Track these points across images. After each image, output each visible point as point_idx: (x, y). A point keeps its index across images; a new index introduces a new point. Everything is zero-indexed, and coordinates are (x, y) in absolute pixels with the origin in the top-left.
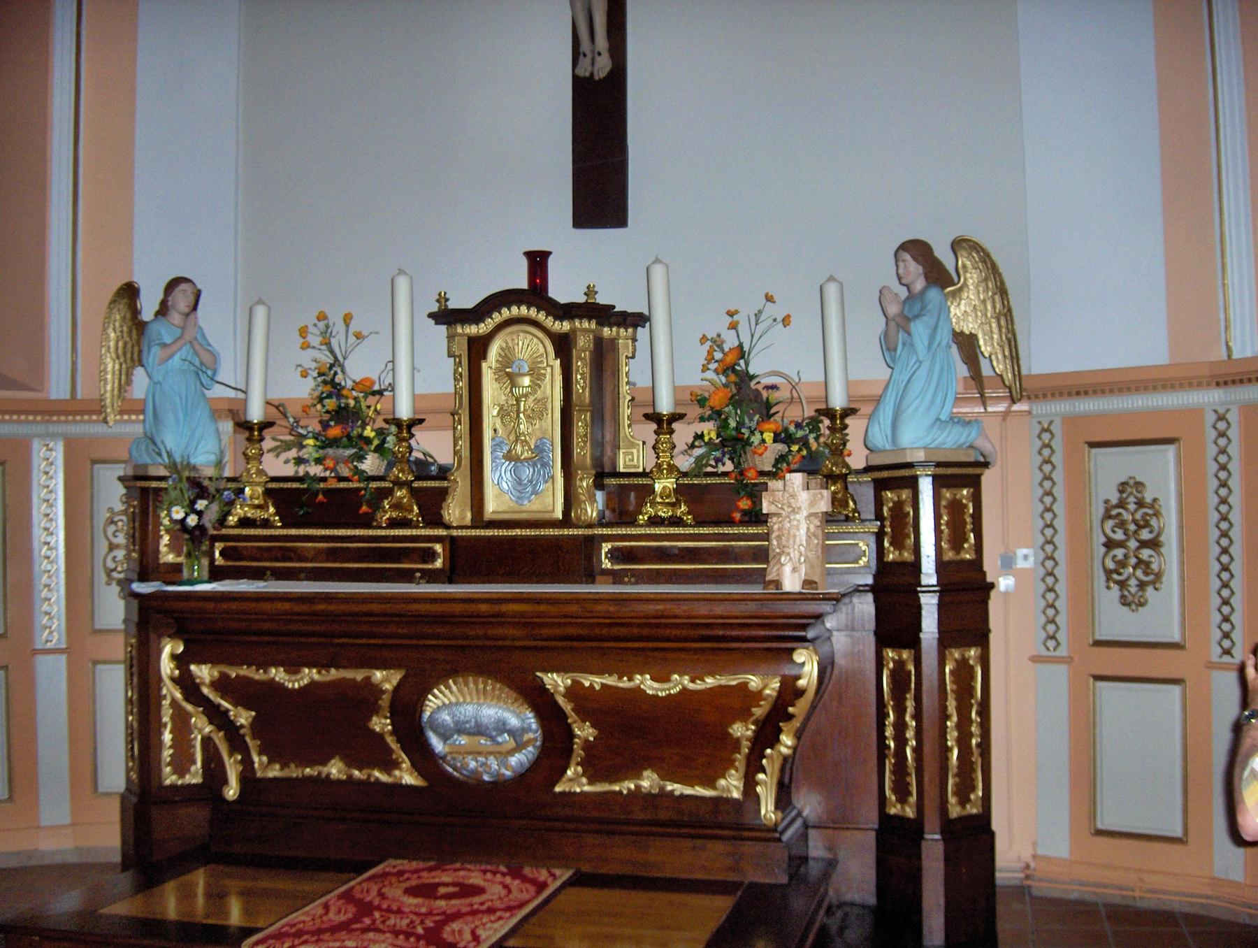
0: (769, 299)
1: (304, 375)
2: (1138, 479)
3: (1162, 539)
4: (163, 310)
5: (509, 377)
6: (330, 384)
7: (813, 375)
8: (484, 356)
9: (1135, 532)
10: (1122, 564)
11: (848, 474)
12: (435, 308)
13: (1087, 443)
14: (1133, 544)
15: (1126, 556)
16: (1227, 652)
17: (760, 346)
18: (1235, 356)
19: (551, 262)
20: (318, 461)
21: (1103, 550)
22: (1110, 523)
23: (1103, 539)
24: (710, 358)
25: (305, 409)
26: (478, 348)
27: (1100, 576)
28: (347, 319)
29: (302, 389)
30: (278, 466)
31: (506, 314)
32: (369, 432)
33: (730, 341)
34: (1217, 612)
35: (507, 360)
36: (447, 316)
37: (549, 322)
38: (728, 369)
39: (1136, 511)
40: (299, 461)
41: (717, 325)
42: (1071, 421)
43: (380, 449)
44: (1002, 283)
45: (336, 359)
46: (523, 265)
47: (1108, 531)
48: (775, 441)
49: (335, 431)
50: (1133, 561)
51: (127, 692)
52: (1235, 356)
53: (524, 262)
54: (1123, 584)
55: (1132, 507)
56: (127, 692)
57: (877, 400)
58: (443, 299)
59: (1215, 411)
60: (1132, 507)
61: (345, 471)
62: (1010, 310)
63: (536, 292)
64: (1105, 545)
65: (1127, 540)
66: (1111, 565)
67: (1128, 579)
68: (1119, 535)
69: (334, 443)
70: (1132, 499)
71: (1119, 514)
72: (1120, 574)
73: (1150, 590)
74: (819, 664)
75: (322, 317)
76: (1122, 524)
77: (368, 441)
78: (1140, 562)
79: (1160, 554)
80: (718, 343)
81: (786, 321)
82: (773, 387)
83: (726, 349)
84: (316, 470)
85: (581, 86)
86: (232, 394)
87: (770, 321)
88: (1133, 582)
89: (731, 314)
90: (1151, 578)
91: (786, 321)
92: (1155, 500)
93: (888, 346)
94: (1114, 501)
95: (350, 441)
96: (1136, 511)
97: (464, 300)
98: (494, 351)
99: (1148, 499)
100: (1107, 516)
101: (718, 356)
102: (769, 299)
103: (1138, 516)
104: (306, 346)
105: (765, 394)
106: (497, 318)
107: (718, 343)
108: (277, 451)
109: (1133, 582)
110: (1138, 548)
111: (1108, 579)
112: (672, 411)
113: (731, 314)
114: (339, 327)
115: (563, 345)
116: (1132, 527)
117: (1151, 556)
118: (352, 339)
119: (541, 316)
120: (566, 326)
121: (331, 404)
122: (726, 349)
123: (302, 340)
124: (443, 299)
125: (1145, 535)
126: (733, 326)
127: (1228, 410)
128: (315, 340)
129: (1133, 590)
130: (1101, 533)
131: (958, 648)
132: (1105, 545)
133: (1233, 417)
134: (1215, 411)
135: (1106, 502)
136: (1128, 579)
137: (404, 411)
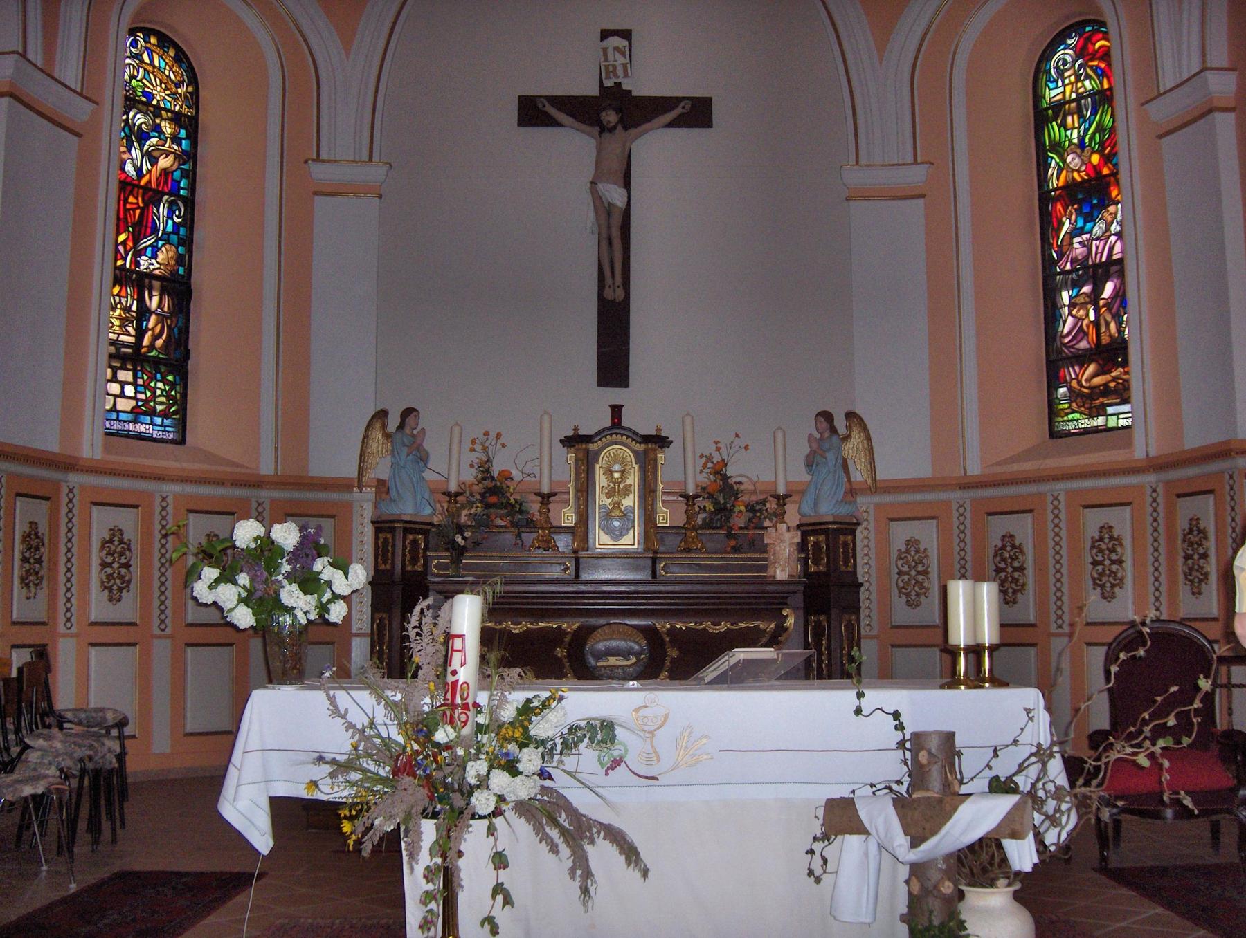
0: (737, 436)
2: (1110, 524)
3: (1208, 553)
4: (401, 427)
7: (767, 477)
9: (1108, 555)
10: (908, 583)
13: (987, 513)
14: (1107, 562)
15: (1104, 570)
16: (1060, 627)
17: (732, 460)
18: (969, 473)
19: (623, 409)
21: (897, 576)
22: (1095, 551)
23: (897, 570)
24: (705, 466)
27: (895, 591)
28: (499, 436)
29: (469, 475)
33: (717, 459)
38: (716, 472)
39: (915, 555)
41: (710, 449)
42: (1069, 493)
44: (869, 434)
45: (489, 457)
47: (900, 566)
48: (747, 511)
50: (914, 582)
52: (969, 473)
53: (609, 410)
54: (907, 595)
55: (1106, 540)
57: (802, 493)
59: (958, 502)
60: (1106, 540)
62: (872, 448)
64: (898, 574)
65: (910, 571)
66: (901, 584)
67: (910, 592)
68: (906, 568)
70: (913, 549)
71: (905, 557)
72: (906, 589)
73: (1019, 595)
76: (1004, 560)
78: (1111, 572)
79: (1024, 574)
80: (709, 458)
81: (746, 448)
82: (740, 483)
83: (715, 462)
86: (439, 478)
87: (737, 447)
88: (913, 593)
89: (717, 443)
90: (1117, 581)
91: (746, 448)
92: (925, 549)
93: (810, 463)
94: (903, 550)
96: (915, 555)
99: (1017, 544)
100: (1093, 547)
101: (710, 465)
102: (737, 436)
103: (1110, 546)
104: (473, 450)
105: (735, 487)
107: (709, 458)
109: (913, 593)
110: (1013, 572)
111: (1095, 584)
112: (694, 493)
113: (717, 443)
116: (913, 564)
117: (1117, 569)
118: (499, 446)
122: (715, 462)
123: (471, 446)
125: (920, 568)
126: (718, 449)
127: (965, 502)
129: (1108, 589)
130: (1089, 556)
132: (898, 574)
133: (968, 506)
134: (958, 502)
135: (1093, 538)
136: (910, 592)
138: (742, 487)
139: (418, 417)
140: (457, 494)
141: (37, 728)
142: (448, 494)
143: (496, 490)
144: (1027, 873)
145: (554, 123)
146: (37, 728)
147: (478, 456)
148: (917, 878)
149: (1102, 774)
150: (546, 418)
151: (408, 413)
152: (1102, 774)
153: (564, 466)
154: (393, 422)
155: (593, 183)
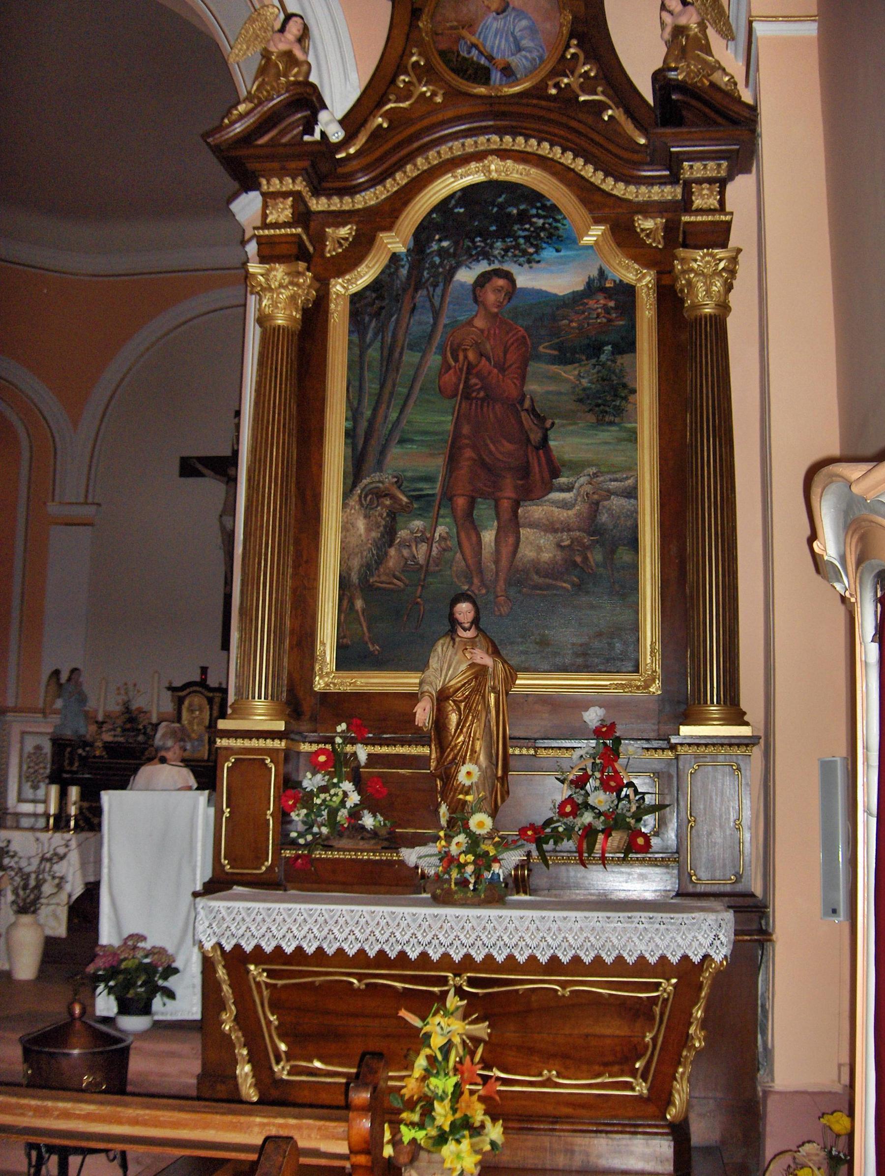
1: (118, 704)
4: (69, 680)
5: (191, 711)
6: (127, 709)
8: (183, 703)
11: (618, 795)
12: (167, 685)
19: (209, 671)
20: (122, 736)
25: (117, 717)
26: (180, 702)
28: (135, 685)
30: (108, 737)
31: (191, 689)
32: (141, 727)
34: (836, 1068)
35: (190, 705)
36: (171, 688)
37: (206, 693)
40: (115, 736)
43: (145, 734)
46: (199, 671)
49: (128, 726)
51: (876, 592)
56: (876, 592)
58: (170, 683)
61: (131, 740)
63: (203, 683)
69: (128, 730)
74: (553, 364)
75: (126, 684)
77: (140, 730)
84: (121, 739)
85: (225, 594)
95: (133, 730)
97: (178, 683)
98: (186, 703)
104: (119, 694)
106: (188, 690)
108: (107, 731)
114: (131, 687)
115: (210, 701)
119: (203, 691)
120: (211, 695)
121: (127, 716)
124: (170, 683)
128: (122, 692)
131: (283, 263)
137: (154, 720)
138: (556, 233)
139: (79, 675)
140: (103, 723)
141: (260, 697)
142: (97, 722)
143: (132, 720)
144: (409, 867)
145: (200, 475)
146: (260, 697)
147: (121, 698)
148: (244, 237)
149: (649, 1053)
150: (157, 675)
151: (74, 671)
152: (649, 1053)
153: (167, 705)
154: (64, 677)
155: (221, 516)
